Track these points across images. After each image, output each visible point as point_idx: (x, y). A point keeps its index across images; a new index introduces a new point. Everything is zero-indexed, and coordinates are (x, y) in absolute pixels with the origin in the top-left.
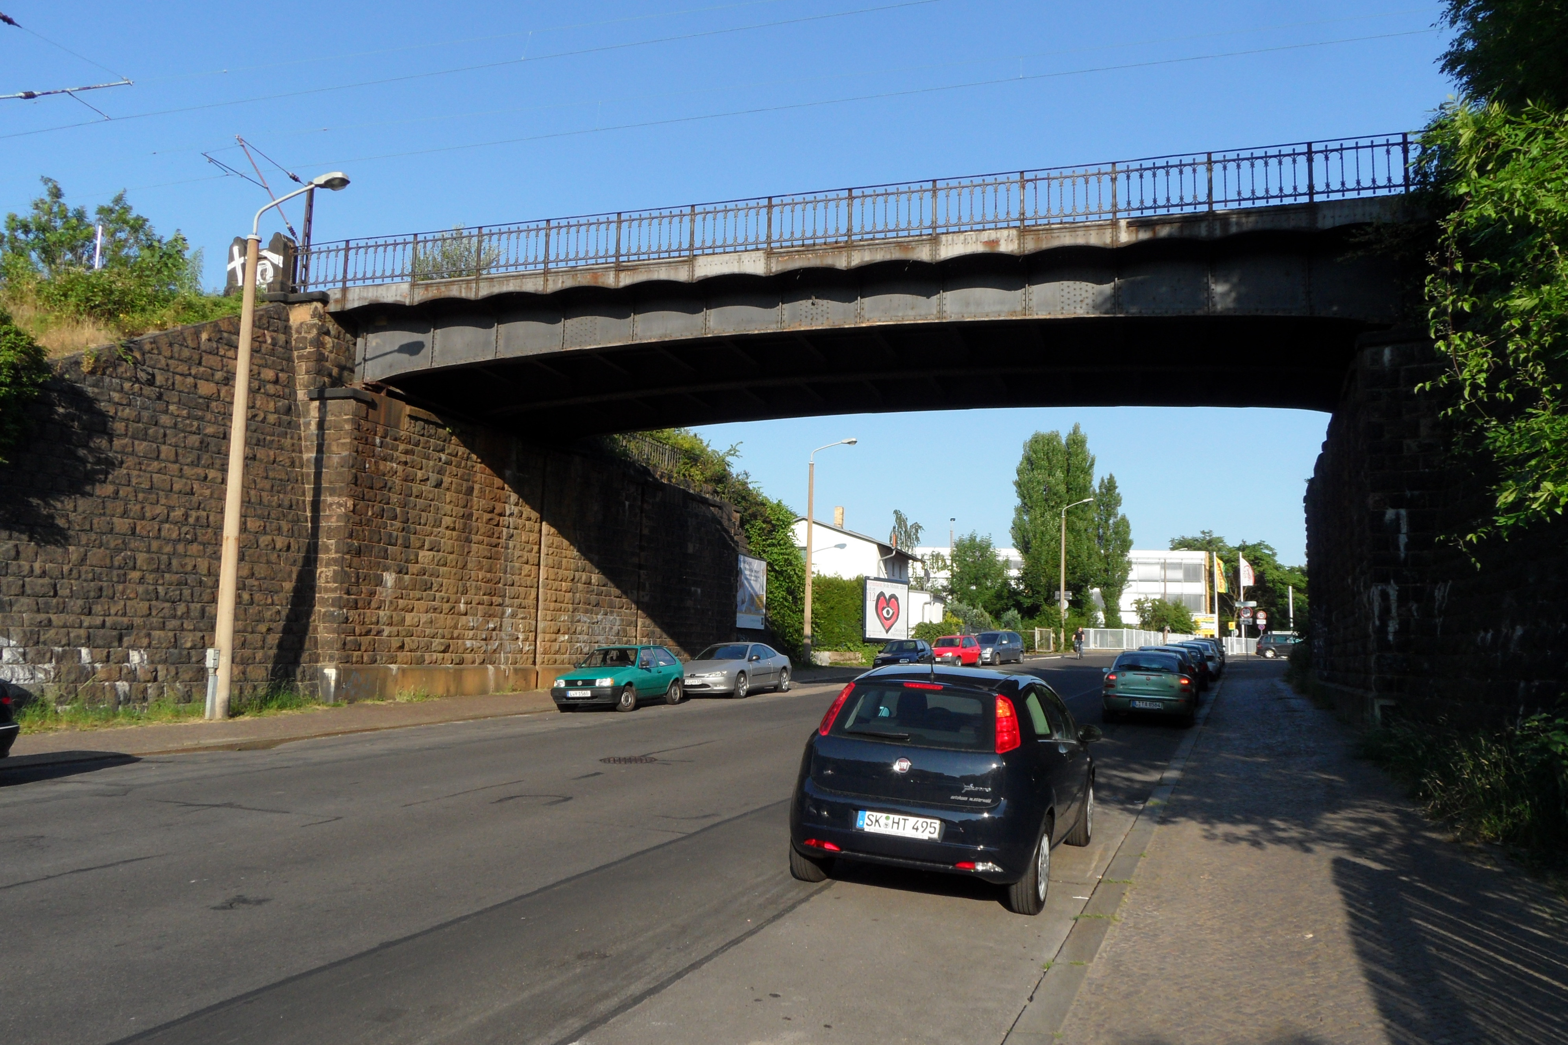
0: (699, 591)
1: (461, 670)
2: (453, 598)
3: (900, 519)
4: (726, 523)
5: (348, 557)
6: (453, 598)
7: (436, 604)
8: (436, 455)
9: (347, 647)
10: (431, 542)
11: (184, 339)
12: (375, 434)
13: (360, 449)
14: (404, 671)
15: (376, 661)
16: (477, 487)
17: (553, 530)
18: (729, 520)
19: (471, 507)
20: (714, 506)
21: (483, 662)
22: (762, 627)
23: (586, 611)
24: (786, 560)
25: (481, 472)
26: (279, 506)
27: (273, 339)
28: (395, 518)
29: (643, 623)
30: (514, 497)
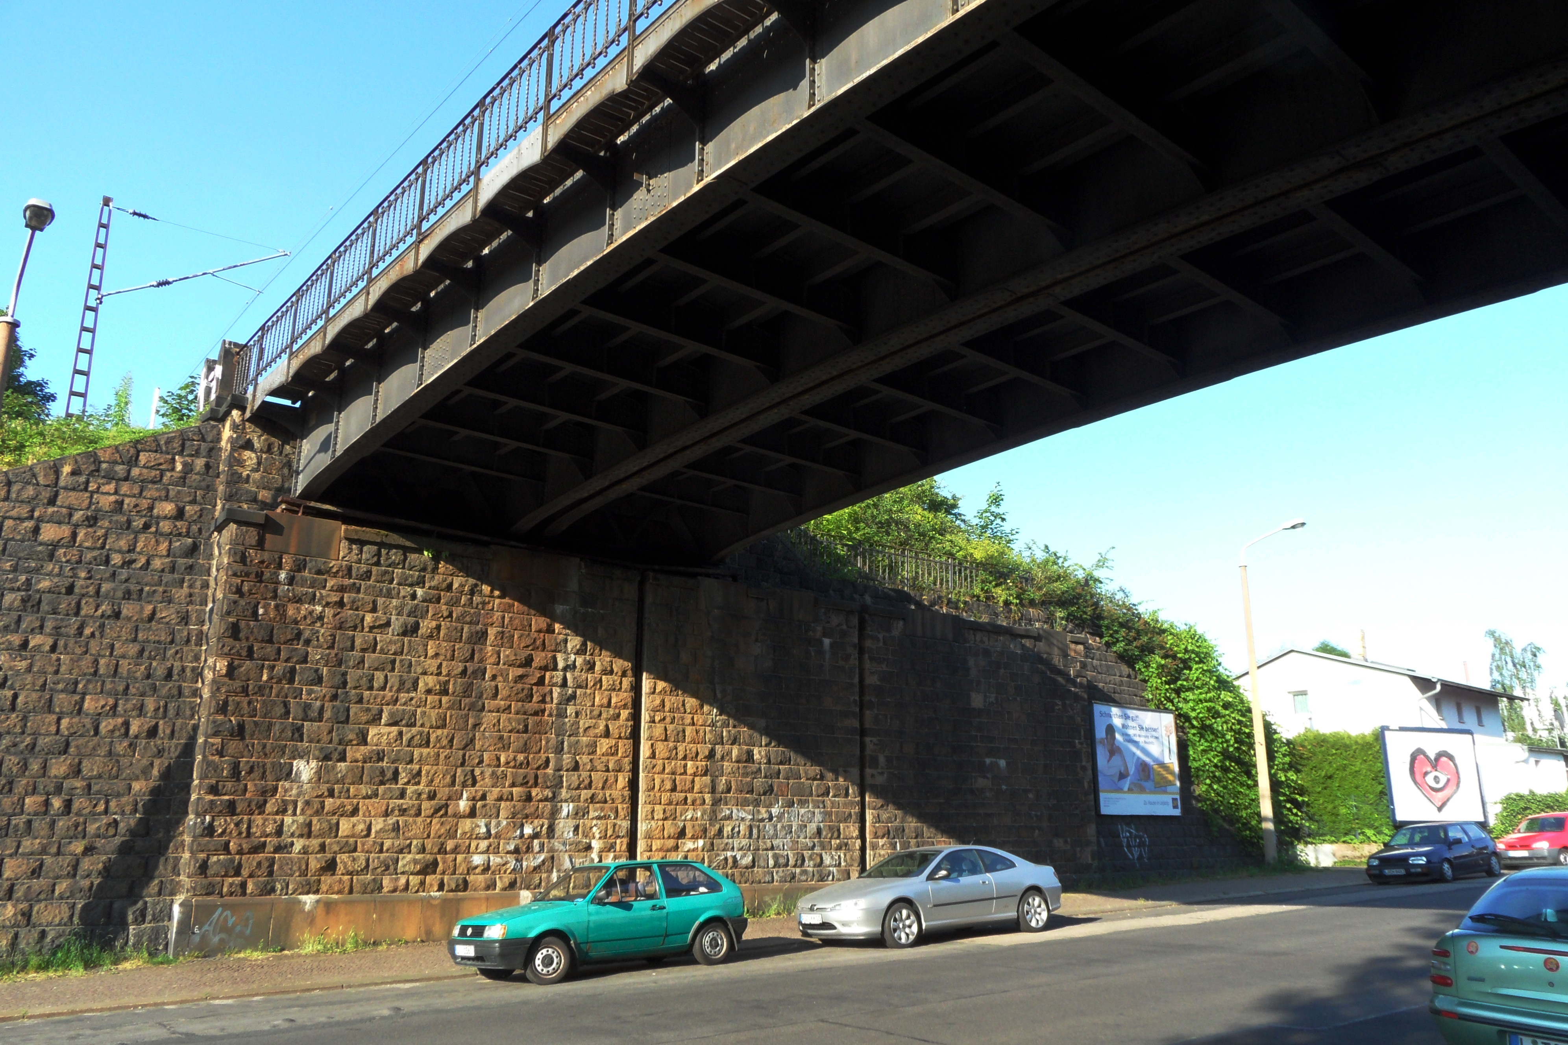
0: (1002, 763)
1: (459, 901)
2: (443, 793)
3: (1502, 646)
4: (1057, 661)
5: (217, 740)
6: (443, 793)
7: (405, 803)
8: (406, 591)
9: (210, 872)
10: (392, 714)
11: (34, 476)
12: (280, 566)
13: (245, 588)
14: (329, 906)
15: (273, 890)
16: (492, 632)
17: (661, 685)
18: (1065, 655)
19: (481, 661)
20: (1027, 637)
21: (512, 885)
22: (1177, 812)
23: (744, 803)
24: (1209, 710)
25: (498, 608)
26: (148, 676)
27: (185, 464)
28: (319, 680)
29: (878, 819)
30: (574, 642)
